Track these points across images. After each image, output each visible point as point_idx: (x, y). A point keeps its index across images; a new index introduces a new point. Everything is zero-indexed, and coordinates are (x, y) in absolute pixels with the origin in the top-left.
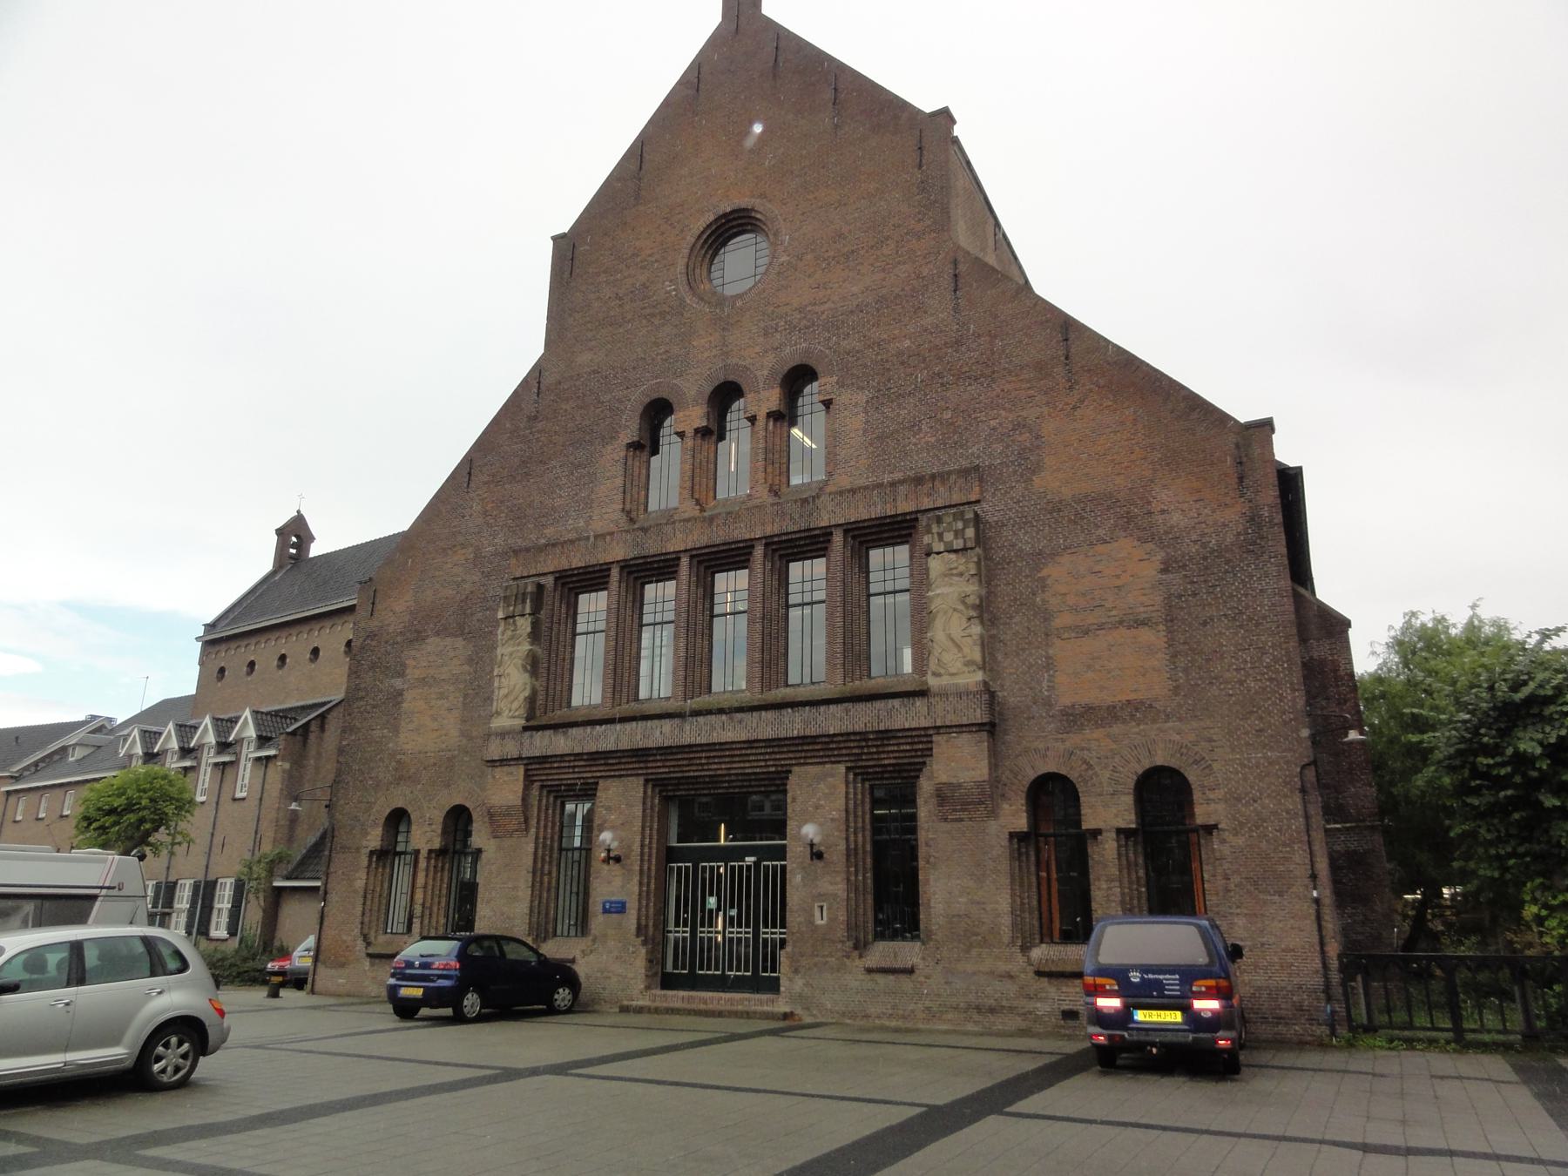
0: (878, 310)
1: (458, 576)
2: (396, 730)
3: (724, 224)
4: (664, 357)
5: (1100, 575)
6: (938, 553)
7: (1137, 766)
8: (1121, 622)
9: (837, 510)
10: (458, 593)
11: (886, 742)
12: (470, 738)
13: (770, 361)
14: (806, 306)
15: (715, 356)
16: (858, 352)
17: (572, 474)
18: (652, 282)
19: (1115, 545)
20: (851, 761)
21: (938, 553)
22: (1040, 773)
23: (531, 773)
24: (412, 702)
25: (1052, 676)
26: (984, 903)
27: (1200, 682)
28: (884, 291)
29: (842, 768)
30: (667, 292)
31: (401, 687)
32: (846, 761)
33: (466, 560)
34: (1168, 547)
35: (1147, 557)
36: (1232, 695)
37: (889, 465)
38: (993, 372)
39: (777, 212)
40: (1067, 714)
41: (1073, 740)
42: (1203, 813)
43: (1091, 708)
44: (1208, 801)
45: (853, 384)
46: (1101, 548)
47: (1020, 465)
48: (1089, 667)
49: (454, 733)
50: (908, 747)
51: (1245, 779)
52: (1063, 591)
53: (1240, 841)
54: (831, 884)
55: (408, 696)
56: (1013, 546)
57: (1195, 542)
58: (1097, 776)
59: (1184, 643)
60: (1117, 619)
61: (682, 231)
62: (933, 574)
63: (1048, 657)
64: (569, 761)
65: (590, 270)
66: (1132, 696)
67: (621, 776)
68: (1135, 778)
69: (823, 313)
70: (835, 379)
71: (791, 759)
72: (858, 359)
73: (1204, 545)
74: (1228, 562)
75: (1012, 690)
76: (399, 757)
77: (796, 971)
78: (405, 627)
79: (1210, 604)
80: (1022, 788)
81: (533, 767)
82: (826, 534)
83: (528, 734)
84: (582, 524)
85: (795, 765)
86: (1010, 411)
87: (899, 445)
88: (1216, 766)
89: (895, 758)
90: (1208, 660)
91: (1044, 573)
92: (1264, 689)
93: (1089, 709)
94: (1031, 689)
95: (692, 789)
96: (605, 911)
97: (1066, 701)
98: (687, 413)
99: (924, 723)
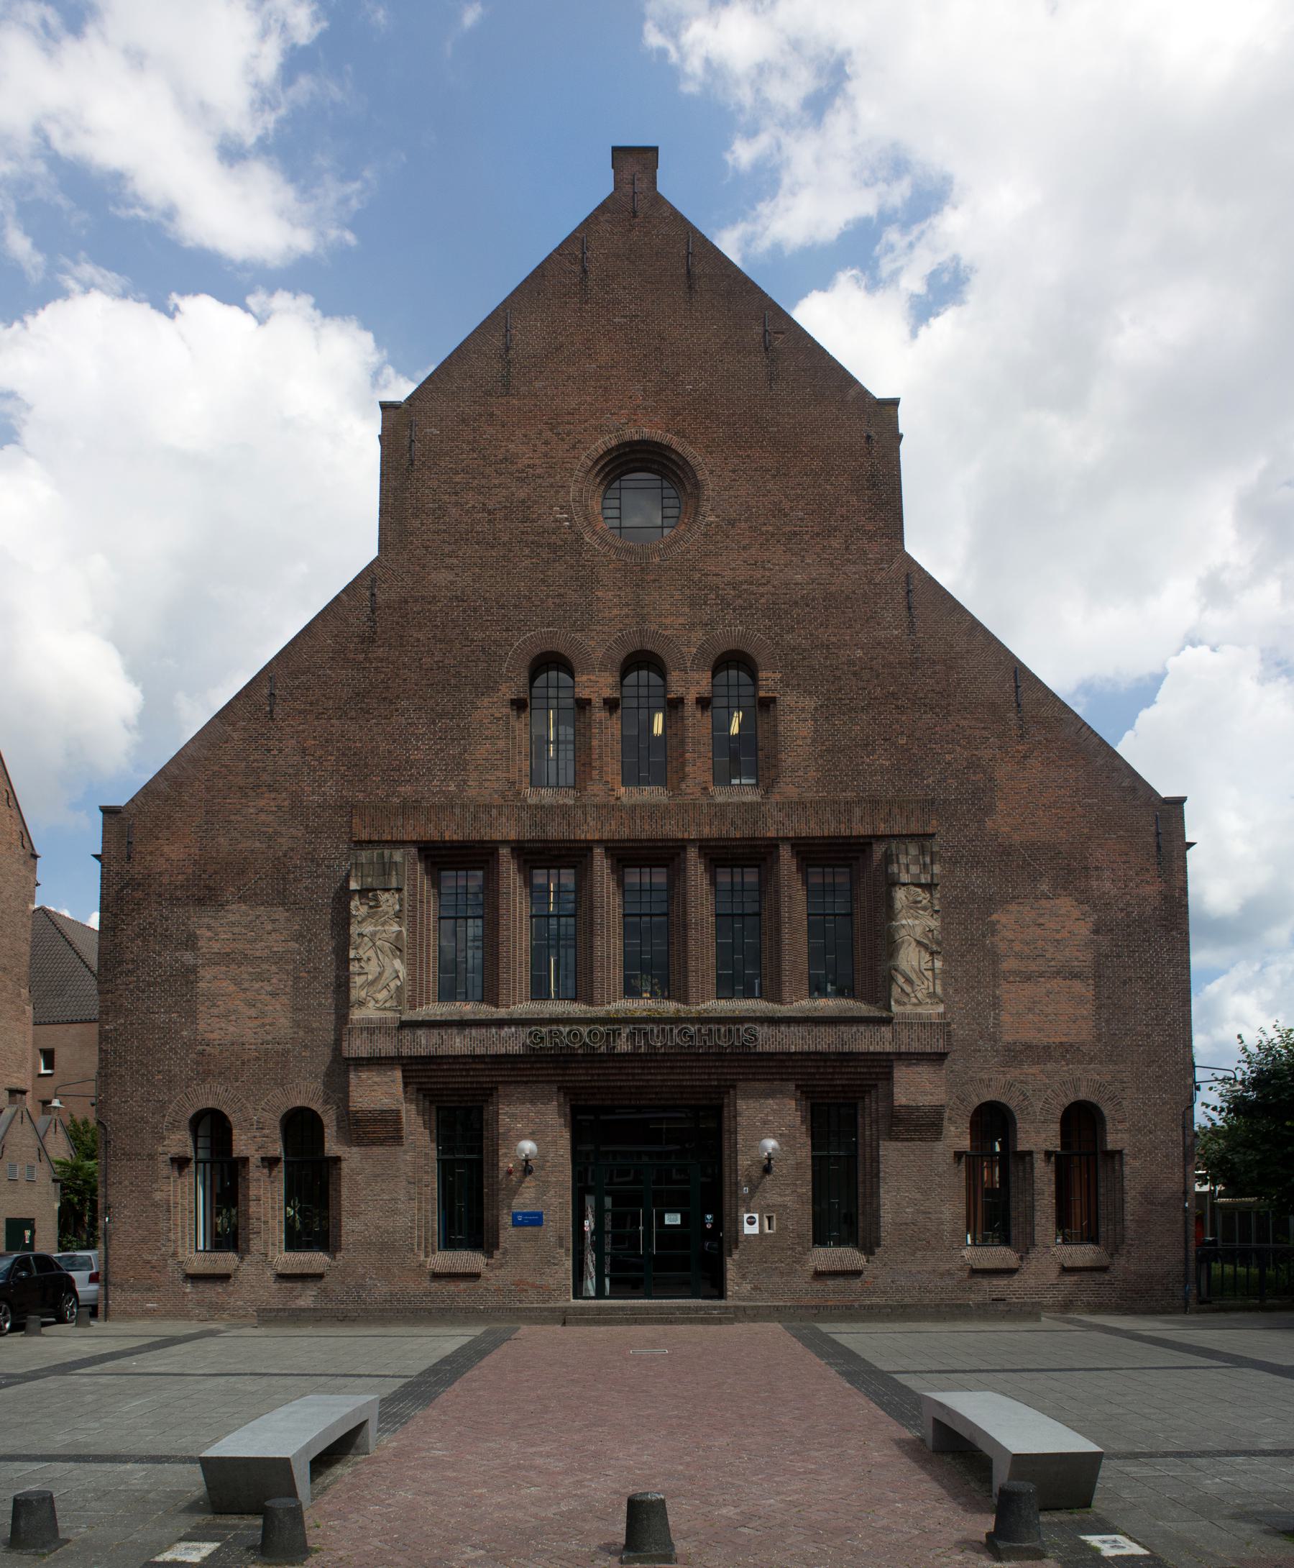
0: (826, 609)
1: (268, 826)
2: (192, 1015)
3: (625, 454)
4: (557, 601)
5: (1042, 927)
6: (904, 884)
7: (1065, 1100)
8: (1058, 973)
9: (787, 823)
10: (269, 847)
11: (845, 1064)
12: (309, 1030)
13: (698, 636)
14: (741, 583)
15: (627, 616)
16: (804, 650)
17: (435, 724)
18: (535, 502)
19: (1057, 901)
20: (802, 1079)
21: (904, 884)
22: (983, 1101)
23: (408, 1074)
24: (208, 979)
25: (998, 1014)
26: (930, 1213)
27: (1117, 1032)
28: (833, 589)
29: (792, 1086)
30: (556, 521)
31: (192, 962)
32: (798, 1079)
33: (279, 807)
34: (1100, 911)
35: (1083, 917)
36: (1141, 1046)
37: (841, 783)
38: (949, 705)
39: (700, 459)
40: (1009, 1050)
41: (1013, 1073)
42: (1114, 1139)
43: (1029, 1046)
44: (1117, 1131)
45: (799, 685)
46: (1043, 902)
47: (973, 804)
48: (1030, 1009)
49: (283, 1022)
50: (865, 1070)
51: (1145, 1115)
52: (1011, 937)
53: (1137, 1164)
54: (781, 1195)
55: (207, 973)
56: (966, 888)
57: (1122, 910)
58: (1033, 1106)
59: (1109, 998)
60: (1055, 969)
61: (574, 447)
62: (898, 905)
63: (995, 997)
64: (465, 1063)
65: (443, 464)
66: (1064, 1039)
67: (526, 1082)
68: (1063, 1110)
69: (762, 595)
70: (778, 676)
71: (739, 1073)
72: (804, 658)
73: (1128, 914)
74: (1146, 932)
75: (961, 1024)
76: (200, 1048)
77: (744, 1277)
78: (187, 880)
79: (1130, 966)
80: (967, 1113)
81: (414, 1067)
82: (771, 846)
83: (406, 1032)
84: (452, 788)
85: (740, 1080)
86: (964, 747)
87: (851, 763)
88: (1125, 1103)
89: (847, 1079)
90: (1125, 1015)
91: (994, 917)
92: (1165, 1042)
93: (1028, 1047)
94: (978, 1024)
95: (696, 1080)
96: (516, 1224)
97: (1008, 1038)
98: (593, 678)
99: (888, 1048)
